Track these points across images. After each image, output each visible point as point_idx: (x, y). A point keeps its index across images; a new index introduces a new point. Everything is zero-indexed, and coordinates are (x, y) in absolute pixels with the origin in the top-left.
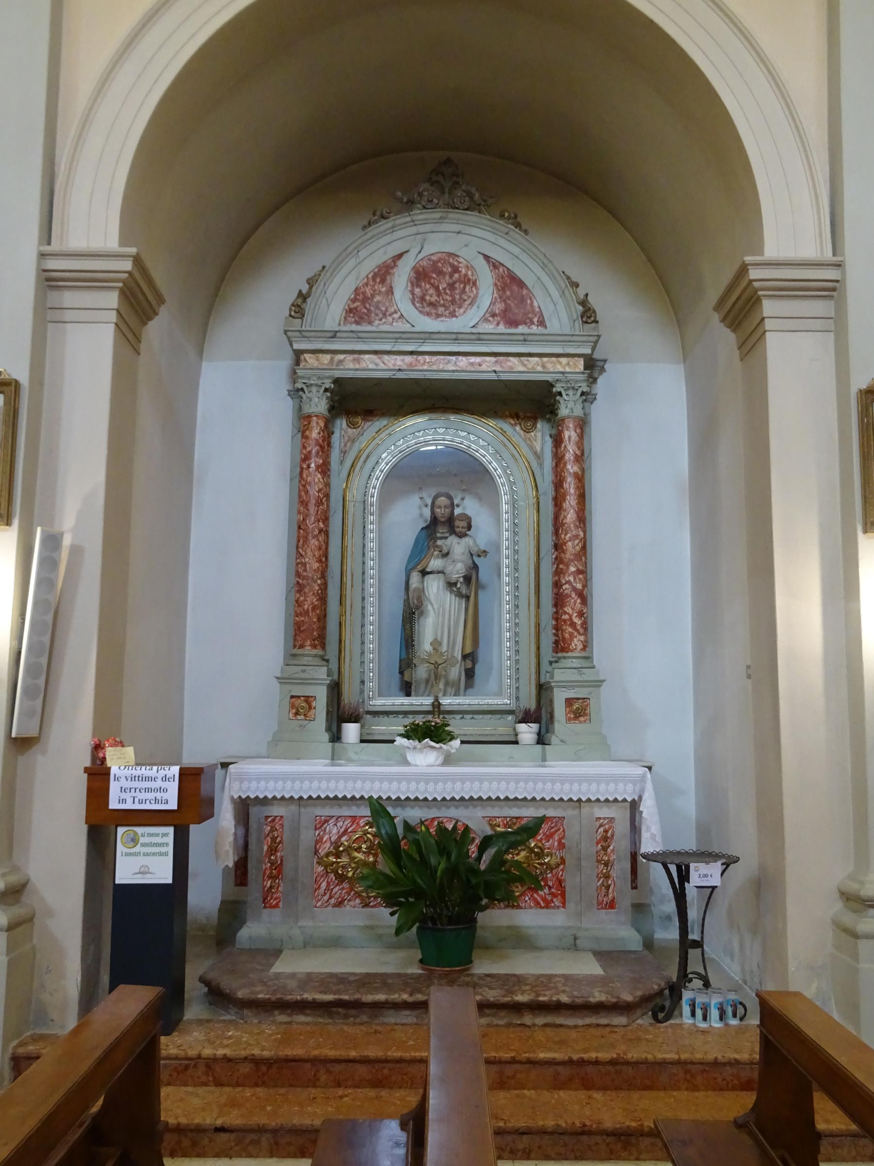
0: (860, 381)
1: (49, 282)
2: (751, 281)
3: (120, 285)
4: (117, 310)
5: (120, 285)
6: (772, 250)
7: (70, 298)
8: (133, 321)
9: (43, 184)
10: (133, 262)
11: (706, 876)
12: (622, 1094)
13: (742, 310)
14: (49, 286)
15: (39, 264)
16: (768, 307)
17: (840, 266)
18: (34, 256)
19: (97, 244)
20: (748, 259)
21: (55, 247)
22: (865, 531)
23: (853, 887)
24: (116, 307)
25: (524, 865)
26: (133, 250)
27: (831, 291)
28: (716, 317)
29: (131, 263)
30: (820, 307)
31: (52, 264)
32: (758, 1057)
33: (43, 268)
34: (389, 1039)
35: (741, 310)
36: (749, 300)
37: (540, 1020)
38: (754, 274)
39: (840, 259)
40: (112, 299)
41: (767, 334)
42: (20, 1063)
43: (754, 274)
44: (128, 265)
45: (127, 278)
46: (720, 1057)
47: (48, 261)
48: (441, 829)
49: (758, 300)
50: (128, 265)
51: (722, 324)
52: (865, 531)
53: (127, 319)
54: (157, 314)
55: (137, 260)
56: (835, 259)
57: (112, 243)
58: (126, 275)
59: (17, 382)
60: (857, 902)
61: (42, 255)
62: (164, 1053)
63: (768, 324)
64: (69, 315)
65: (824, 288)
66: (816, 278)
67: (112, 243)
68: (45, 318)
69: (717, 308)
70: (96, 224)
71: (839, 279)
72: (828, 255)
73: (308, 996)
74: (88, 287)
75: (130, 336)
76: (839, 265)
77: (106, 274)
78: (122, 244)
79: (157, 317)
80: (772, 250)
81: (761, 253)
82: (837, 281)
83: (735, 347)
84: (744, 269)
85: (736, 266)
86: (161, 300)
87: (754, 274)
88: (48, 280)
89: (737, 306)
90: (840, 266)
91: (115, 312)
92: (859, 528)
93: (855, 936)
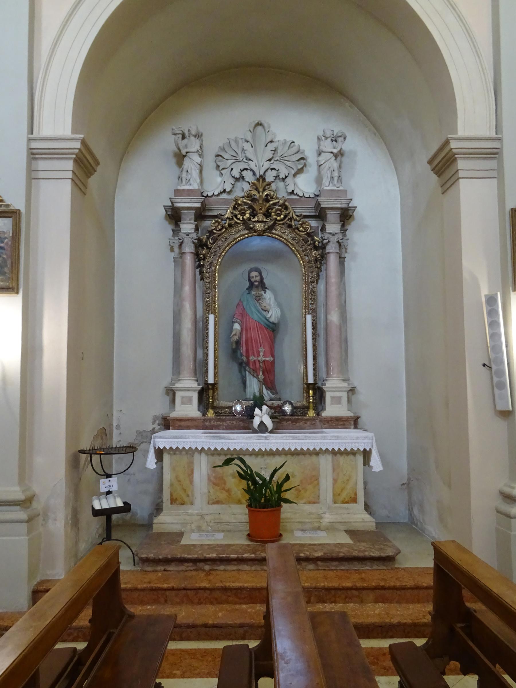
0: (510, 205)
1: (33, 155)
2: (452, 149)
3: (74, 156)
4: (73, 171)
5: (74, 156)
6: (461, 132)
7: (42, 165)
10: (81, 143)
12: (404, 605)
13: (444, 165)
14: (33, 158)
15: (28, 145)
16: (461, 164)
17: (500, 140)
18: (25, 140)
20: (449, 136)
21: (35, 135)
23: (507, 490)
24: (72, 169)
27: (494, 154)
28: (429, 167)
30: (492, 164)
31: (34, 145)
32: (432, 584)
33: (30, 147)
34: (246, 578)
35: (444, 165)
37: (222, 567)
38: (453, 145)
39: (500, 136)
40: (70, 165)
42: (37, 594)
43: (453, 145)
44: (78, 145)
46: (175, 586)
47: (32, 143)
49: (455, 159)
50: (78, 145)
53: (80, 178)
55: (83, 142)
56: (497, 136)
58: (77, 150)
59: (19, 210)
60: (508, 498)
61: (29, 140)
62: (123, 586)
63: (461, 174)
65: (491, 153)
68: (32, 177)
70: (58, 121)
73: (246, 555)
74: (62, 158)
77: (487, 150)
80: (461, 132)
84: (447, 142)
85: (443, 140)
86: (98, 164)
87: (453, 145)
88: (33, 154)
89: (440, 165)
90: (500, 140)
91: (71, 172)
92: (511, 288)
93: (508, 516)
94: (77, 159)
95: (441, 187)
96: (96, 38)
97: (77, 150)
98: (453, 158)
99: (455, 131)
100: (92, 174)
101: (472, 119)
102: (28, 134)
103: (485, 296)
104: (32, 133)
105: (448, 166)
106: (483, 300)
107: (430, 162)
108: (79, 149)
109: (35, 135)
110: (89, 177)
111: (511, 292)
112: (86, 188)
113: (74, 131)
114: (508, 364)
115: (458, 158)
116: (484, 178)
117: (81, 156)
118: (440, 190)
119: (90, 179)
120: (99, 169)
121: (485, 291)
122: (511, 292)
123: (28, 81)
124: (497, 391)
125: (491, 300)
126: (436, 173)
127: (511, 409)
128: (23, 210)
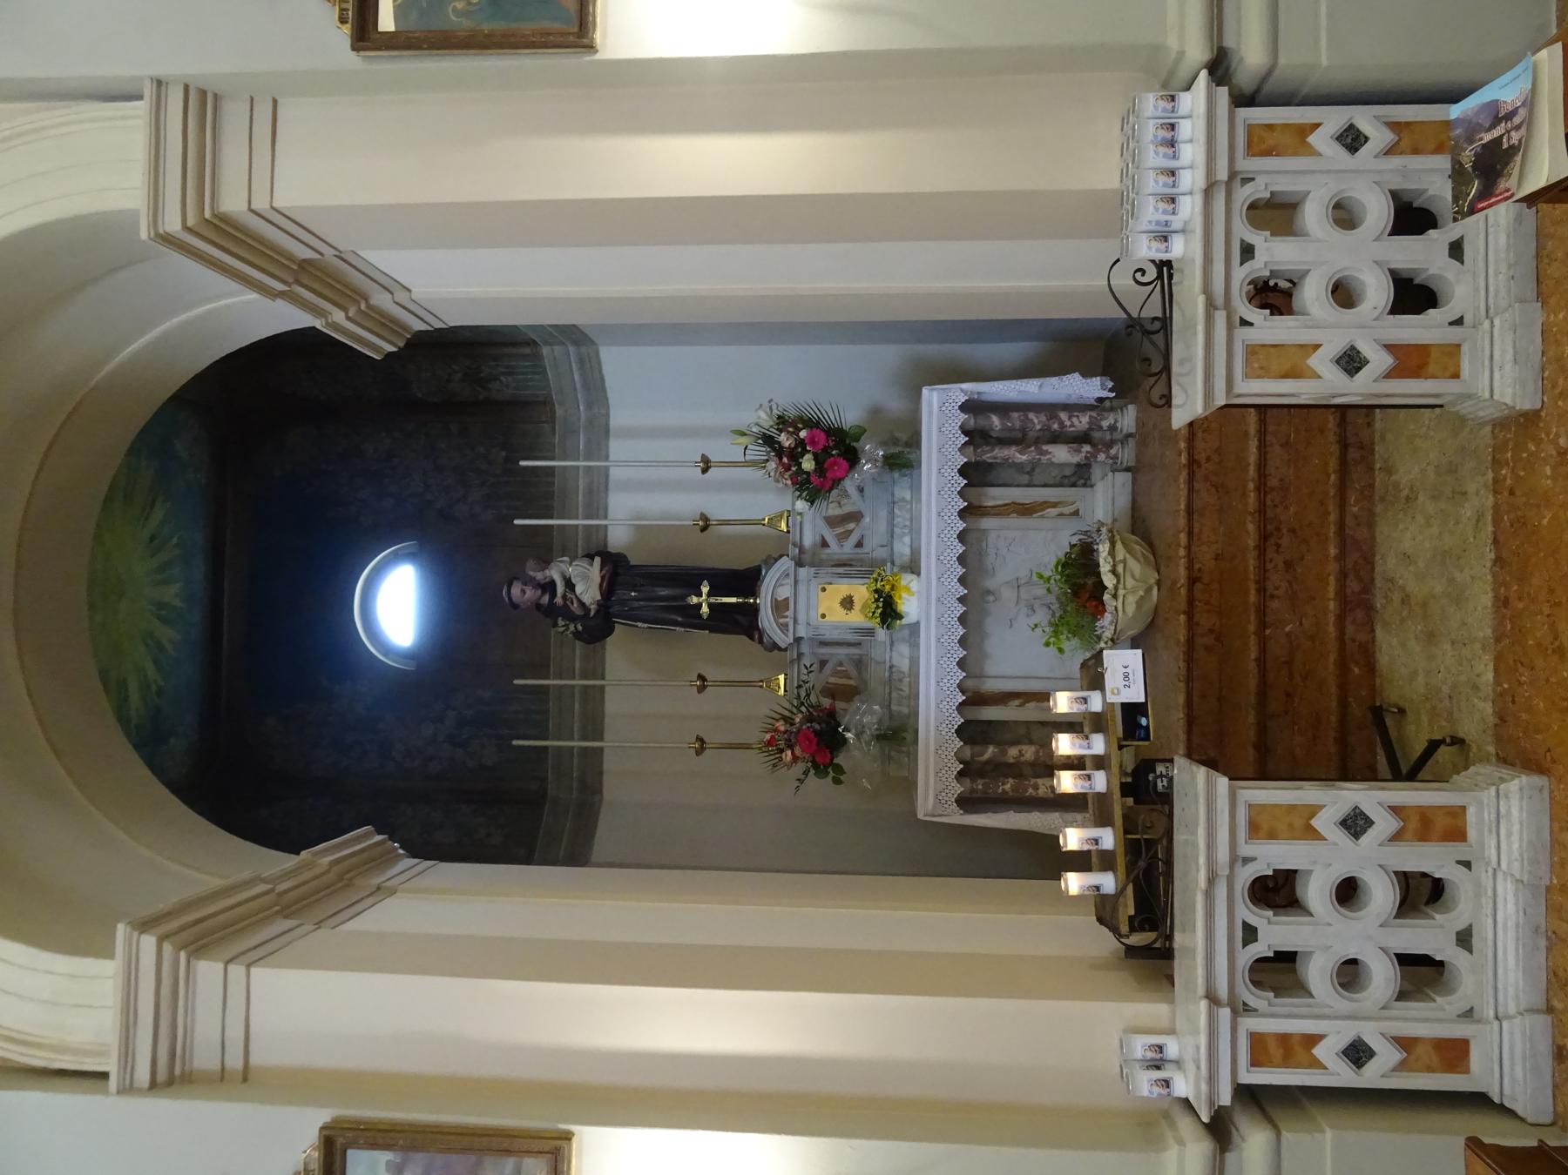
1: (174, 1078)
2: (186, 228)
5: (183, 955)
11: (1126, 677)
16: (233, 202)
20: (144, 235)
25: (1158, 945)
27: (204, 104)
30: (234, 119)
31: (143, 1075)
35: (242, 918)
38: (172, 223)
40: (208, 971)
44: (148, 942)
49: (224, 218)
50: (148, 942)
55: (144, 926)
59: (322, 1129)
61: (127, 1089)
65: (201, 114)
66: (179, 193)
68: (240, 1079)
71: (181, 88)
72: (141, 108)
78: (108, 954)
81: (135, 213)
82: (186, 88)
87: (172, 223)
91: (231, 967)
94: (192, 947)
97: (167, 948)
99: (130, 218)
102: (106, 1092)
104: (104, 1076)
108: (161, 940)
109: (111, 1065)
113: (104, 951)
115: (212, 208)
116: (248, 999)
128: (324, 1116)
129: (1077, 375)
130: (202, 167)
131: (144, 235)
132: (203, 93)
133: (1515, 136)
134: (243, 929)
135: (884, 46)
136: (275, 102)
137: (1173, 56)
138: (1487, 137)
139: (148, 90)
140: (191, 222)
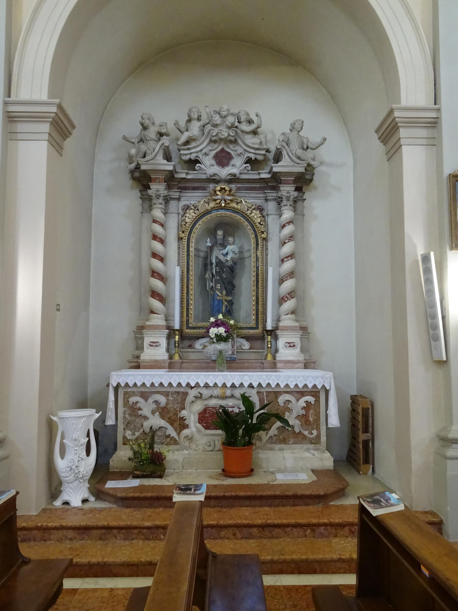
1: (11, 118)
2: (395, 118)
3: (51, 120)
4: (49, 133)
5: (51, 120)
6: (404, 103)
8: (56, 136)
9: (410, 549)
10: (57, 107)
13: (388, 132)
14: (9, 121)
16: (403, 132)
19: (36, 97)
21: (13, 98)
22: (452, 249)
26: (57, 101)
27: (434, 124)
28: (376, 136)
29: (56, 108)
31: (12, 108)
36: (395, 126)
40: (46, 127)
41: (403, 146)
44: (54, 109)
45: (54, 116)
48: (225, 411)
49: (398, 128)
50: (54, 109)
51: (379, 140)
52: (250, 472)
53: (55, 138)
54: (71, 134)
55: (60, 107)
56: (436, 106)
57: (44, 96)
58: (54, 114)
59: (451, 250)
61: (6, 103)
63: (402, 141)
64: (20, 136)
67: (44, 96)
69: (377, 132)
75: (56, 146)
76: (439, 110)
79: (71, 136)
80: (404, 103)
82: (438, 118)
83: (385, 153)
84: (391, 112)
86: (74, 127)
87: (396, 114)
92: (448, 247)
95: (386, 154)
96: (49, 87)
98: (396, 127)
99: (399, 102)
100: (67, 137)
101: (413, 92)
103: (421, 255)
104: (9, 96)
105: (391, 136)
106: (420, 258)
107: (377, 132)
108: (56, 113)
109: (13, 98)
110: (65, 140)
111: (448, 250)
112: (62, 149)
113: (51, 94)
114: (443, 318)
115: (402, 127)
117: (57, 118)
118: (385, 158)
119: (66, 142)
120: (75, 132)
121: (421, 251)
122: (448, 250)
123: (6, 53)
124: (433, 343)
125: (426, 259)
126: (382, 142)
127: (445, 359)
129: (108, 482)
130: (412, 123)
131: (393, 106)
132: (436, 123)
133: (384, 504)
134: (393, 133)
135: (450, 324)
136: (435, 145)
137: (343, 475)
138: (382, 500)
139: (437, 106)
140: (397, 119)
